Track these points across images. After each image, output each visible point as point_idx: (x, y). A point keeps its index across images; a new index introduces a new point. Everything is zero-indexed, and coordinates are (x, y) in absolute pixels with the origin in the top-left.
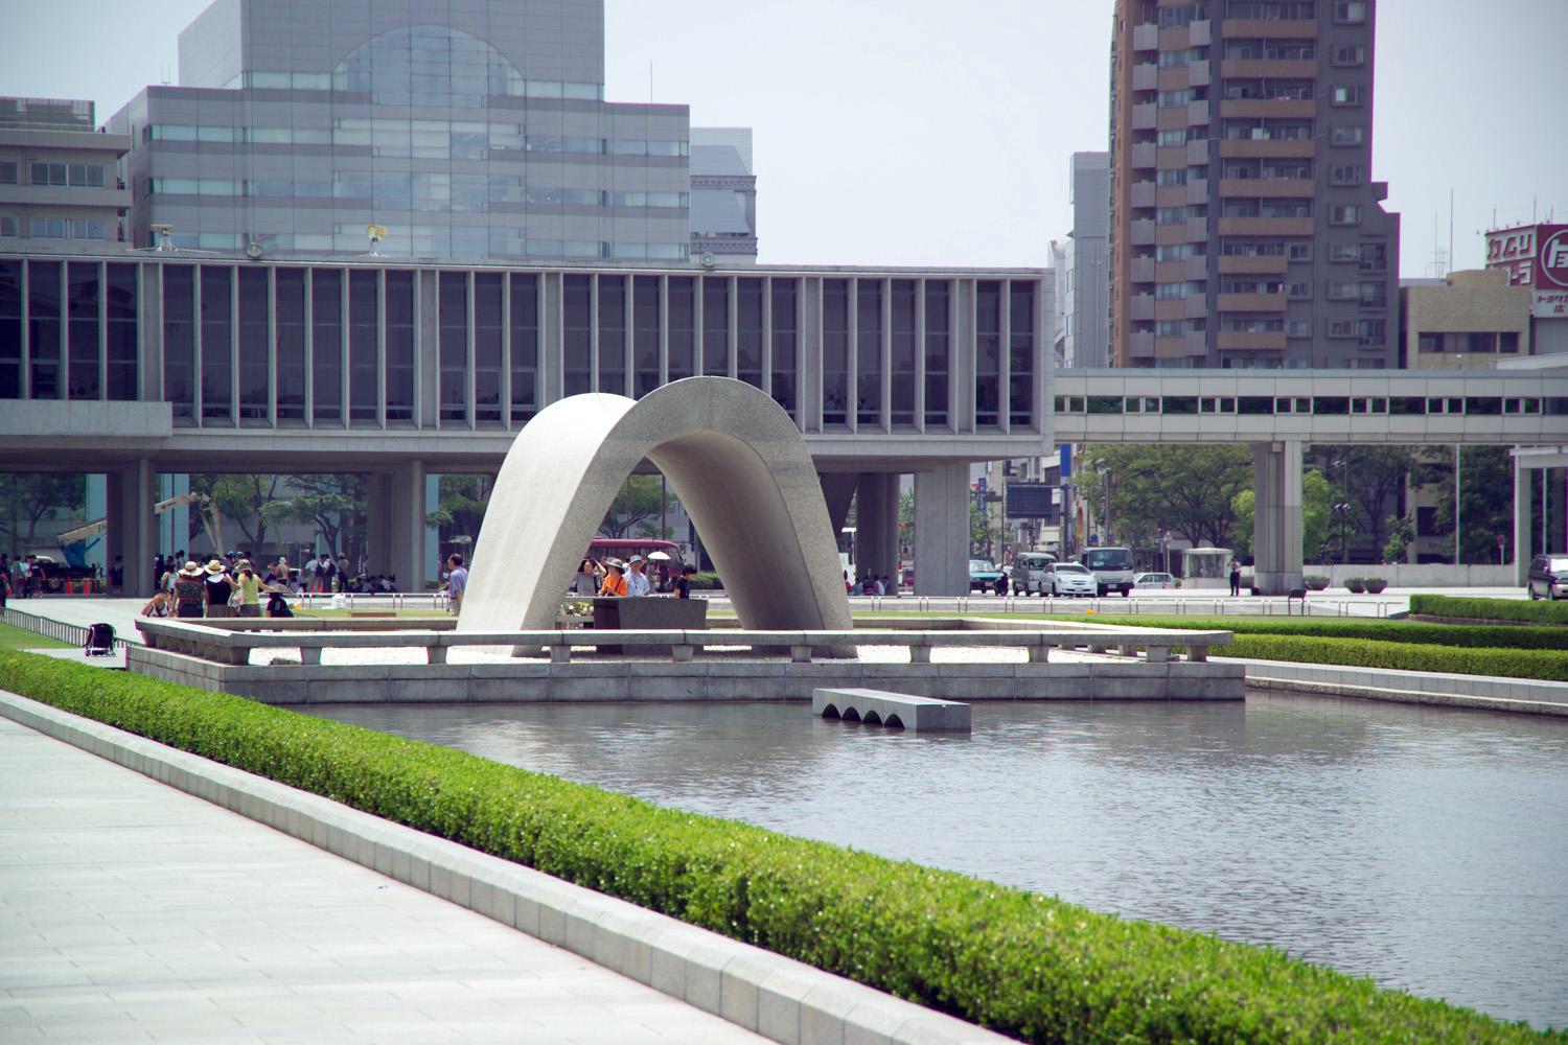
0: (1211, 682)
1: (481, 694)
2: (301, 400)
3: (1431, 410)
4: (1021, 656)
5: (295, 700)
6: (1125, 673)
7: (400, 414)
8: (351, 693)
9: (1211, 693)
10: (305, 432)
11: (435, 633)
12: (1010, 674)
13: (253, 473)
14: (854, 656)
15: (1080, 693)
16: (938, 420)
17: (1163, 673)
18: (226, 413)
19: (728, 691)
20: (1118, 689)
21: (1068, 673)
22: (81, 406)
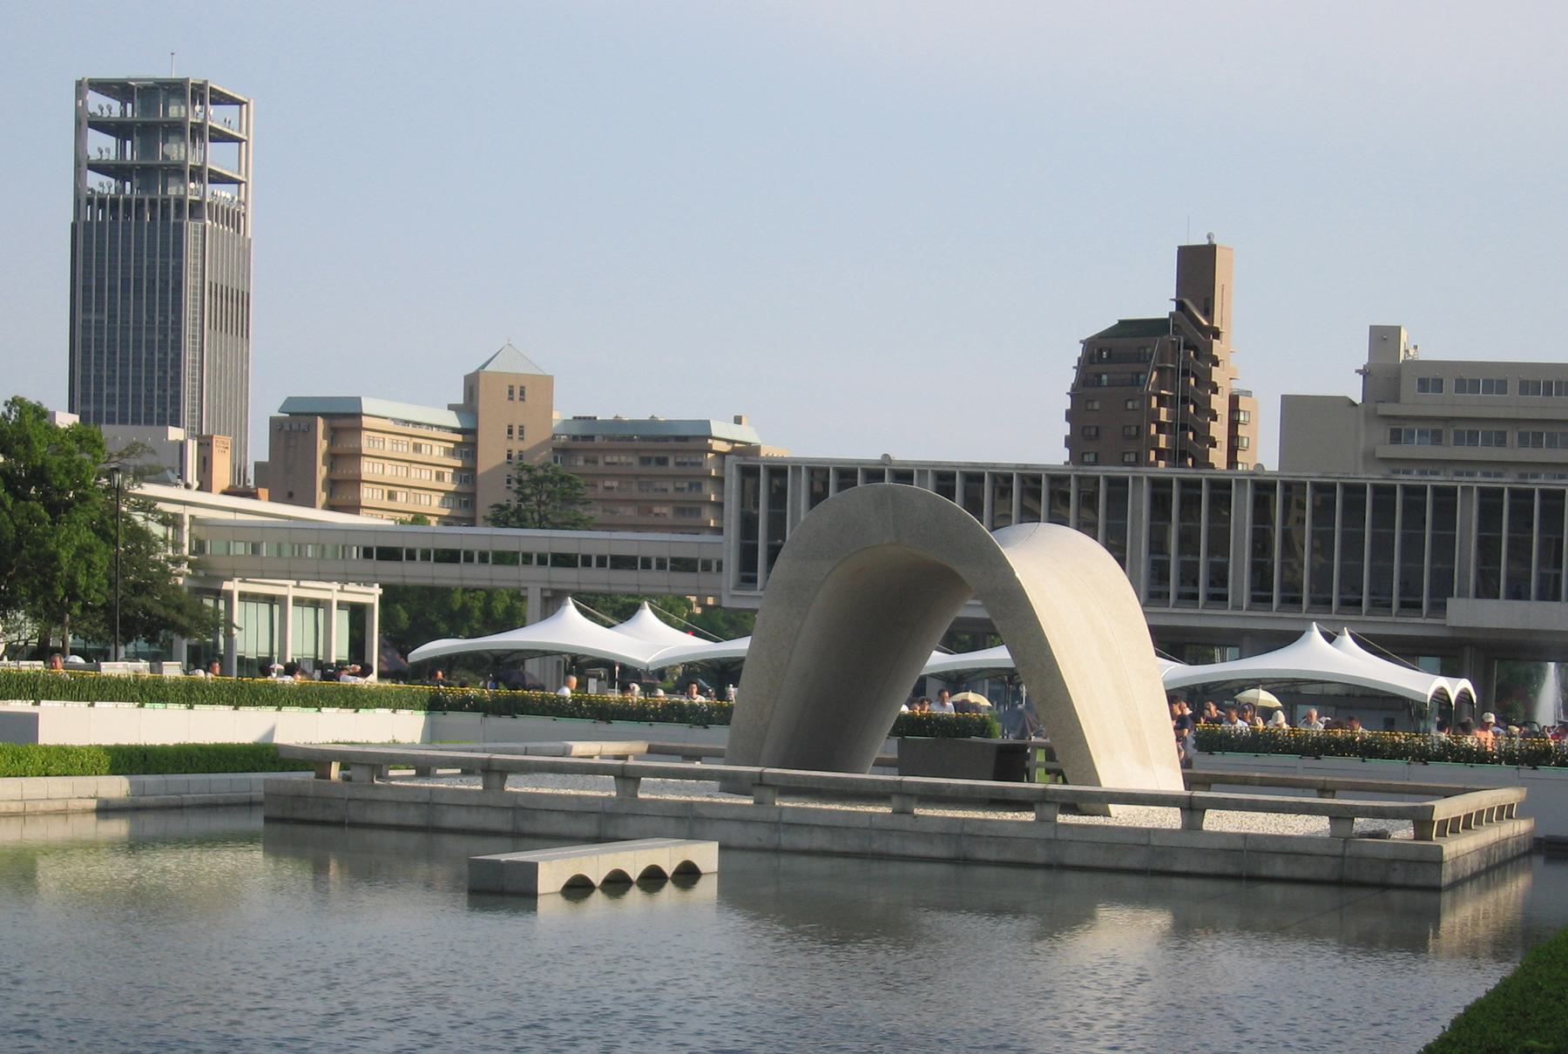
0: (1397, 865)
1: (527, 826)
2: (1299, 589)
3: (605, 558)
4: (1318, 825)
5: (333, 819)
6: (1289, 849)
7: (1219, 598)
8: (390, 816)
9: (1397, 878)
10: (1166, 610)
11: (486, 756)
12: (1144, 841)
13: (1219, 646)
14: (1107, 814)
15: (1231, 870)
16: (1219, 598)
17: (1338, 851)
18: (1419, 606)
19: (803, 840)
20: (1279, 868)
21: (1223, 844)
22: (1519, 605)
